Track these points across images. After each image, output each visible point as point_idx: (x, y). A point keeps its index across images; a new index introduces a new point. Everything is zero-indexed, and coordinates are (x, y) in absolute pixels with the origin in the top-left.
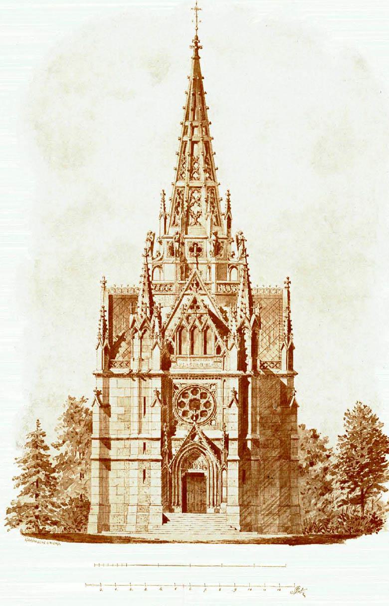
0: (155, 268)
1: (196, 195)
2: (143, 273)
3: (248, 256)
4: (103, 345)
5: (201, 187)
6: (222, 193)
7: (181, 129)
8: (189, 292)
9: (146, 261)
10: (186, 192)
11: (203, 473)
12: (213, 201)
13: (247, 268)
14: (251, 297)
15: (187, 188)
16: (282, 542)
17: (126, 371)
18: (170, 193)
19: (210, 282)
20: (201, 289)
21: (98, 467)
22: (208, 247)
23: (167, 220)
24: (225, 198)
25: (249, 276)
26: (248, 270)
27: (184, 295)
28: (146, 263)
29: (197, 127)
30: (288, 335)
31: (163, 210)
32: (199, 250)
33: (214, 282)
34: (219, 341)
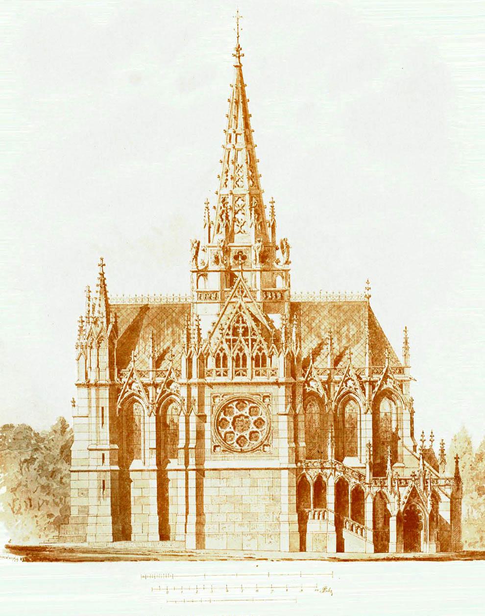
0: (200, 276)
1: (240, 202)
2: (99, 282)
3: (105, 265)
4: (198, 354)
5: (245, 195)
6: (266, 200)
7: (224, 138)
8: (233, 300)
9: (101, 270)
10: (230, 200)
11: (170, 480)
12: (258, 210)
13: (103, 277)
14: (107, 306)
15: (231, 197)
16: (278, 544)
17: (272, 379)
18: (215, 201)
19: (255, 289)
20: (245, 296)
21: (287, 476)
22: (252, 256)
23: (211, 229)
24: (269, 206)
25: (105, 285)
26: (105, 279)
27: (229, 302)
28: (102, 273)
29: (240, 134)
30: (187, 344)
31: (207, 218)
32: (244, 258)
33: (260, 289)
34: (273, 348)
